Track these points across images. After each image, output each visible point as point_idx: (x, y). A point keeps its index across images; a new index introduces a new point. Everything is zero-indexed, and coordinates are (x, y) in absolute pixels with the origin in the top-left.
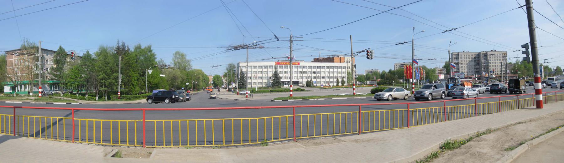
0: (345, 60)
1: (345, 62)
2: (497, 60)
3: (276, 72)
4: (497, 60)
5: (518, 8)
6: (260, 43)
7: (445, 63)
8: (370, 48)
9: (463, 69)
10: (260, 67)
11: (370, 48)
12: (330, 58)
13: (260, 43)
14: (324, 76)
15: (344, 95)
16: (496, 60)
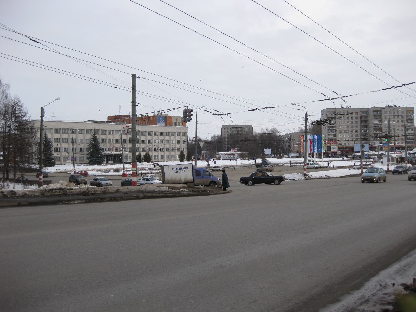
0: (173, 122)
1: (173, 124)
2: (398, 122)
3: (95, 139)
4: (398, 122)
5: (382, 90)
6: (165, 111)
7: (184, 111)
8: (188, 106)
9: (343, 135)
10: (173, 134)
11: (188, 106)
12: (149, 117)
13: (165, 111)
14: (162, 147)
15: (83, 202)
16: (396, 121)
